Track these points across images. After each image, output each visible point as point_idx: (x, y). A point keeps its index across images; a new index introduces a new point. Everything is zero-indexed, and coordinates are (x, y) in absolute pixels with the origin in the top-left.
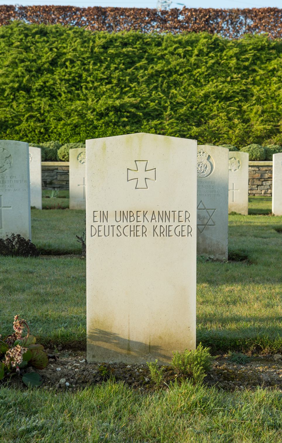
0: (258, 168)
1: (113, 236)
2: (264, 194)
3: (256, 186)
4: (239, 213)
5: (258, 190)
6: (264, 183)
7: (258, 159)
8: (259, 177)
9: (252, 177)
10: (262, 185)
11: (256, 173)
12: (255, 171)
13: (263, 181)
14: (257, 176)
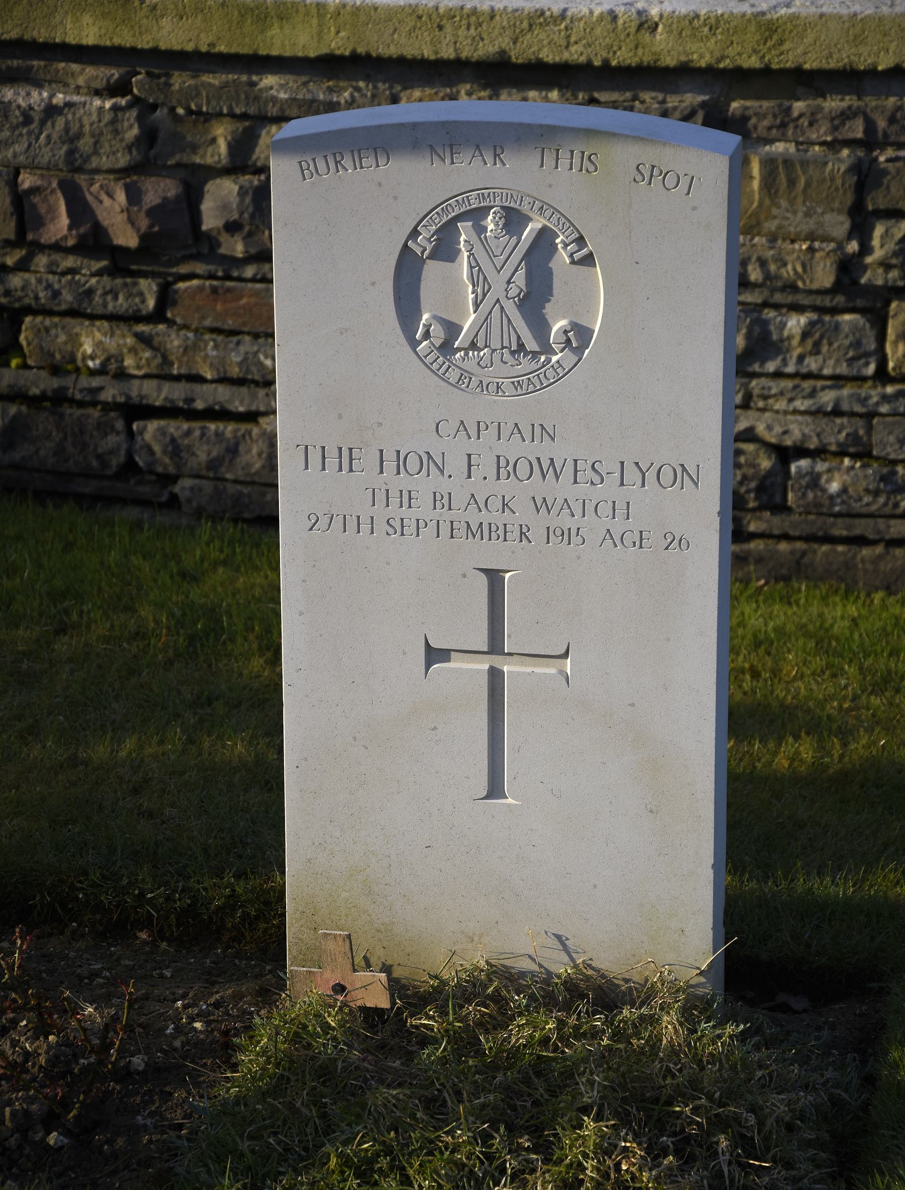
1: (495, 790)
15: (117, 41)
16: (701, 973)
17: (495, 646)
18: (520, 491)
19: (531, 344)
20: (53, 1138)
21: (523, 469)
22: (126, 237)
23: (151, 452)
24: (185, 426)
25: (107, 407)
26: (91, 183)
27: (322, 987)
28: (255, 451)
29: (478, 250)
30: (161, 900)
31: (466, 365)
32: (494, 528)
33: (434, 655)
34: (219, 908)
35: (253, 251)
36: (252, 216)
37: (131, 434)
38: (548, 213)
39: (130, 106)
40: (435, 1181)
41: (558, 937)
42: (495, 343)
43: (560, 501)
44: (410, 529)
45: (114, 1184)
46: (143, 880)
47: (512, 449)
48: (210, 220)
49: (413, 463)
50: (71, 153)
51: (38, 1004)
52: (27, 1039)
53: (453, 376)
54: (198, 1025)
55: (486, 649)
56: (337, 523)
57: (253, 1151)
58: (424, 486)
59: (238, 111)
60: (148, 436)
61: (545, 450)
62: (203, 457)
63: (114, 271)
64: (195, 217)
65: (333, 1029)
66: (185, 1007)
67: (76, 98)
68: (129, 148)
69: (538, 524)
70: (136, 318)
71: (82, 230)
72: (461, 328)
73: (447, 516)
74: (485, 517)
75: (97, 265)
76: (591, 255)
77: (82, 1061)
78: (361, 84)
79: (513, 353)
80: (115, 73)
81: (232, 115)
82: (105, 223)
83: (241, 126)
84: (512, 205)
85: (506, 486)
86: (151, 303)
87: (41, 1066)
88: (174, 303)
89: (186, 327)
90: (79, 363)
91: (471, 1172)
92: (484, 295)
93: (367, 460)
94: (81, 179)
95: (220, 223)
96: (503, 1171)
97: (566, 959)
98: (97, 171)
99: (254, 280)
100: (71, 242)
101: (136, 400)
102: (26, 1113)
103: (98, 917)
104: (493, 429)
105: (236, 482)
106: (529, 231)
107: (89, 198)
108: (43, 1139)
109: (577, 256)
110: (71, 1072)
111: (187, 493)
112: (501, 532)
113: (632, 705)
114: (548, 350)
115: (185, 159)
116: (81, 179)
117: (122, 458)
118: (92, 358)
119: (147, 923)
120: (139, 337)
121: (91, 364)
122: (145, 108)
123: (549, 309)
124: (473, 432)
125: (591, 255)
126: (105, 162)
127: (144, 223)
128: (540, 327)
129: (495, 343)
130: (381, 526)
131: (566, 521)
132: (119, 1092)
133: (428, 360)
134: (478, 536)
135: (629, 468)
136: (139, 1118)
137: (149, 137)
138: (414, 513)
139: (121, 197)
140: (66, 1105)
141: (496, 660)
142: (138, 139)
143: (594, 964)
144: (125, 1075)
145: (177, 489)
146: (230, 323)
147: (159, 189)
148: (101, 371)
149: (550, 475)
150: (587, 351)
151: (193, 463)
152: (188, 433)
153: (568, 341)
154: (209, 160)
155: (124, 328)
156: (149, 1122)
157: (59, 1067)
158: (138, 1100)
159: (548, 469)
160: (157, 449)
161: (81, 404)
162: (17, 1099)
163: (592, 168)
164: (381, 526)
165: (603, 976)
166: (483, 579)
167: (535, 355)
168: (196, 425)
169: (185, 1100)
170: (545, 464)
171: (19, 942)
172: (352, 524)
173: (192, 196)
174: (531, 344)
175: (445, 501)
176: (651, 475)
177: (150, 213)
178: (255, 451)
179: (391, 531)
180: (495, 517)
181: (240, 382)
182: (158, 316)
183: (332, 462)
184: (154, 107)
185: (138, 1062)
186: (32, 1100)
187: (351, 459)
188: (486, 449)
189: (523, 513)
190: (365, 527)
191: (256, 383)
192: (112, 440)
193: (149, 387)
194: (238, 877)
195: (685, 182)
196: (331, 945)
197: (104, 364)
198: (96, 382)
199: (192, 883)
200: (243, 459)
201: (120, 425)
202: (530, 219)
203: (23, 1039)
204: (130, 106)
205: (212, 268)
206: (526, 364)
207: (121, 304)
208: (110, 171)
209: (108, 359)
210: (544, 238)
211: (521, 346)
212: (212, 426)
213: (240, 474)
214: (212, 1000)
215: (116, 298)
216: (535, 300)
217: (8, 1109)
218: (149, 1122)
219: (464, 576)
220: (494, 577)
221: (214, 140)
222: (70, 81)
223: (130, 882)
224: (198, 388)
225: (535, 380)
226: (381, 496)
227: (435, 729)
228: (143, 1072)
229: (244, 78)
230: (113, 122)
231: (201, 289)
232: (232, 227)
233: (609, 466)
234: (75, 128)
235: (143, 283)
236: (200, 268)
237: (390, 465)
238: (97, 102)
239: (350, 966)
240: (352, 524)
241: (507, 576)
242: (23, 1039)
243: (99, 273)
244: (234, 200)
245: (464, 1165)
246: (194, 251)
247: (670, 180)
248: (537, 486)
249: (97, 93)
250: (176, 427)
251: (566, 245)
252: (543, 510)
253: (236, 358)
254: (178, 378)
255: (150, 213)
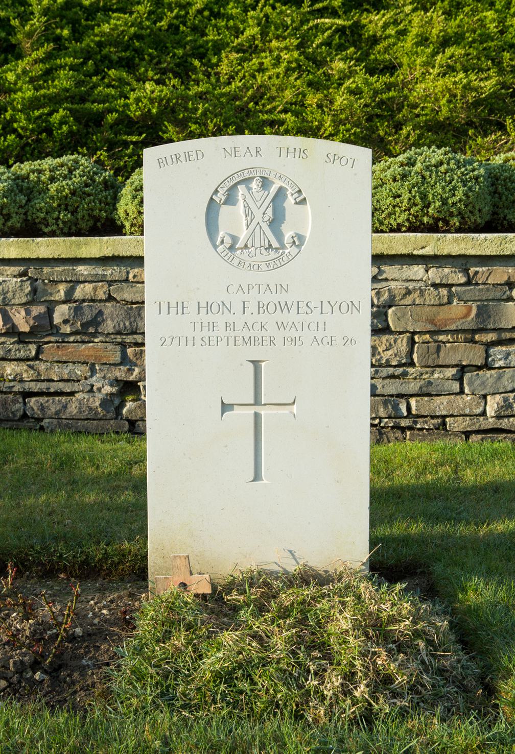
0: (466, 271)
1: (257, 477)
2: (499, 417)
3: (454, 371)
4: (393, 277)
5: (462, 392)
6: (498, 352)
7: (455, 221)
8: (470, 322)
9: (431, 321)
10: (487, 366)
11: (450, 297)
12: (450, 286)
13: (489, 345)
14: (459, 313)
15: (23, 256)
16: (363, 564)
17: (257, 402)
18: (270, 319)
19: (275, 244)
20: (38, 676)
21: (271, 308)
22: (25, 328)
23: (33, 410)
24: (46, 399)
25: (16, 393)
26: (12, 309)
27: (173, 587)
28: (74, 407)
29: (249, 199)
30: (71, 558)
31: (242, 257)
32: (257, 339)
33: (226, 407)
34: (100, 560)
35: (73, 330)
36: (74, 317)
37: (25, 403)
38: (283, 179)
39: (27, 280)
40: (273, 681)
41: (290, 552)
42: (257, 245)
43: (290, 323)
44: (213, 342)
45: (76, 699)
46: (61, 549)
47: (266, 298)
48: (57, 319)
49: (215, 308)
50: (4, 298)
51: (24, 602)
52: (17, 623)
53: (236, 262)
54: (105, 612)
55: (253, 402)
56: (176, 341)
57: (158, 674)
58: (220, 319)
59: (68, 279)
60: (31, 404)
61: (282, 297)
62: (53, 410)
63: (20, 342)
64: (51, 319)
65: (189, 604)
66: (96, 603)
67: (6, 279)
68: (27, 295)
69: (279, 336)
70: (28, 359)
71: (8, 326)
72: (239, 238)
73: (233, 334)
74: (252, 334)
75: (13, 340)
76: (305, 199)
77: (49, 632)
78: (115, 268)
79: (266, 249)
80: (22, 269)
81: (66, 281)
82: (16, 324)
83: (69, 285)
84: (265, 176)
85: (263, 318)
86: (33, 353)
87: (27, 636)
88: (43, 353)
89: (46, 361)
90: (5, 378)
91: (290, 674)
92: (251, 221)
93: (191, 308)
94: (8, 308)
95: (61, 320)
96: (309, 671)
97: (294, 563)
98: (14, 305)
99: (73, 342)
100: (3, 331)
101: (27, 390)
102: (22, 662)
103: (39, 568)
104: (256, 288)
105: (66, 419)
106: (273, 190)
107: (11, 314)
108: (32, 677)
109: (298, 200)
110: (43, 639)
111: (47, 425)
112: (260, 341)
113: (328, 427)
114: (283, 247)
115: (48, 298)
116: (8, 308)
117: (22, 413)
118: (10, 375)
119: (64, 569)
120: (29, 366)
121: (10, 377)
122: (33, 280)
123: (284, 227)
124: (246, 290)
125: (305, 199)
126: (17, 301)
127: (32, 322)
128: (279, 236)
129: (257, 245)
130: (198, 341)
131: (294, 334)
132: (71, 648)
133: (223, 255)
134: (249, 344)
135: (325, 305)
136: (84, 661)
137: (34, 291)
138: (216, 334)
139: (23, 313)
140: (43, 656)
141: (258, 409)
142: (30, 292)
143: (308, 564)
144: (72, 638)
145: (43, 424)
146: (64, 359)
147: (38, 310)
148: (14, 380)
149: (286, 310)
150: (303, 247)
151: (49, 413)
152: (47, 401)
153: (294, 242)
154: (57, 298)
155: (23, 363)
156: (90, 663)
157: (37, 636)
158: (82, 651)
159: (284, 307)
160: (35, 408)
161: (5, 393)
162: (16, 655)
163: (305, 156)
164: (198, 341)
165: (313, 570)
166: (251, 366)
167: (277, 249)
168: (51, 398)
169: (108, 650)
170: (283, 305)
171: (10, 571)
172: (183, 341)
173: (50, 312)
174: (275, 244)
175: (232, 327)
176: (336, 308)
177: (34, 318)
178: (74, 407)
179: (203, 344)
180: (257, 333)
181: (68, 381)
182: (36, 358)
183: (173, 310)
184: (36, 280)
185: (79, 631)
186: (25, 655)
187: (183, 308)
188: (253, 299)
189: (272, 330)
190: (190, 343)
191: (74, 381)
192: (18, 406)
193: (32, 384)
194: (107, 545)
195: (350, 162)
196: (178, 562)
197: (14, 377)
198: (12, 384)
199: (85, 549)
200: (69, 410)
201: (21, 400)
202: (274, 183)
203: (15, 623)
204: (27, 280)
205: (57, 338)
206: (273, 255)
207: (22, 354)
208: (19, 305)
209: (16, 375)
210: (281, 192)
211: (270, 246)
212: (57, 398)
213: (68, 416)
214: (109, 599)
215: (20, 352)
216: (276, 222)
217: (11, 661)
218: (90, 663)
219: (242, 365)
220: (256, 364)
221: (59, 291)
222: (5, 273)
223: (55, 551)
224: (51, 384)
225: (277, 262)
226: (198, 326)
227: (226, 446)
228: (82, 636)
229: (71, 268)
230: (21, 286)
231: (53, 347)
232: (66, 322)
233: (315, 304)
234: (6, 289)
235: (31, 346)
236: (53, 339)
237: (203, 310)
238: (15, 279)
239: (189, 572)
240: (183, 341)
241: (263, 364)
242: (15, 623)
243: (13, 343)
244: (67, 311)
245: (285, 671)
246: (50, 332)
247: (344, 161)
248: (279, 317)
249: (15, 276)
250: (42, 400)
251: (292, 195)
252: (282, 328)
253: (66, 371)
254: (43, 381)
255: (34, 318)
